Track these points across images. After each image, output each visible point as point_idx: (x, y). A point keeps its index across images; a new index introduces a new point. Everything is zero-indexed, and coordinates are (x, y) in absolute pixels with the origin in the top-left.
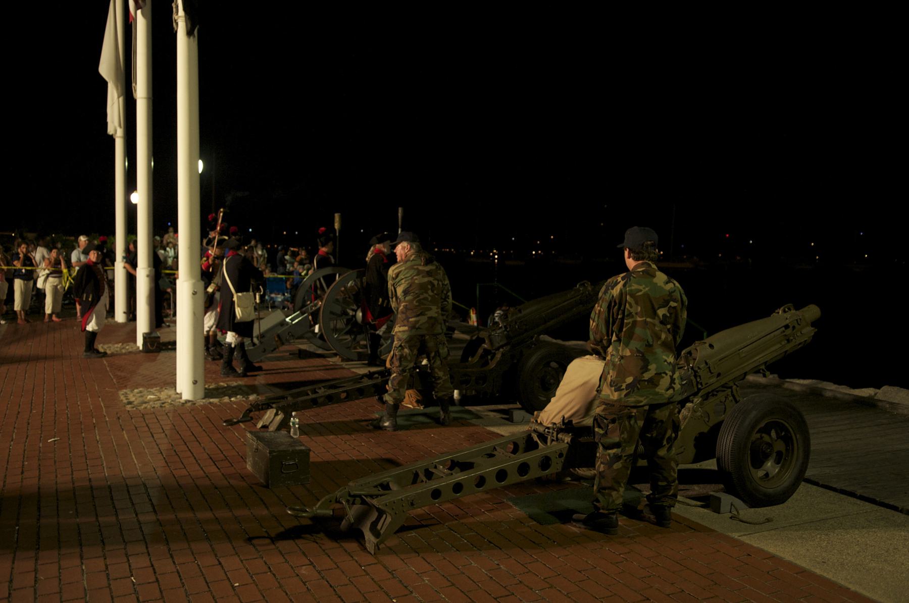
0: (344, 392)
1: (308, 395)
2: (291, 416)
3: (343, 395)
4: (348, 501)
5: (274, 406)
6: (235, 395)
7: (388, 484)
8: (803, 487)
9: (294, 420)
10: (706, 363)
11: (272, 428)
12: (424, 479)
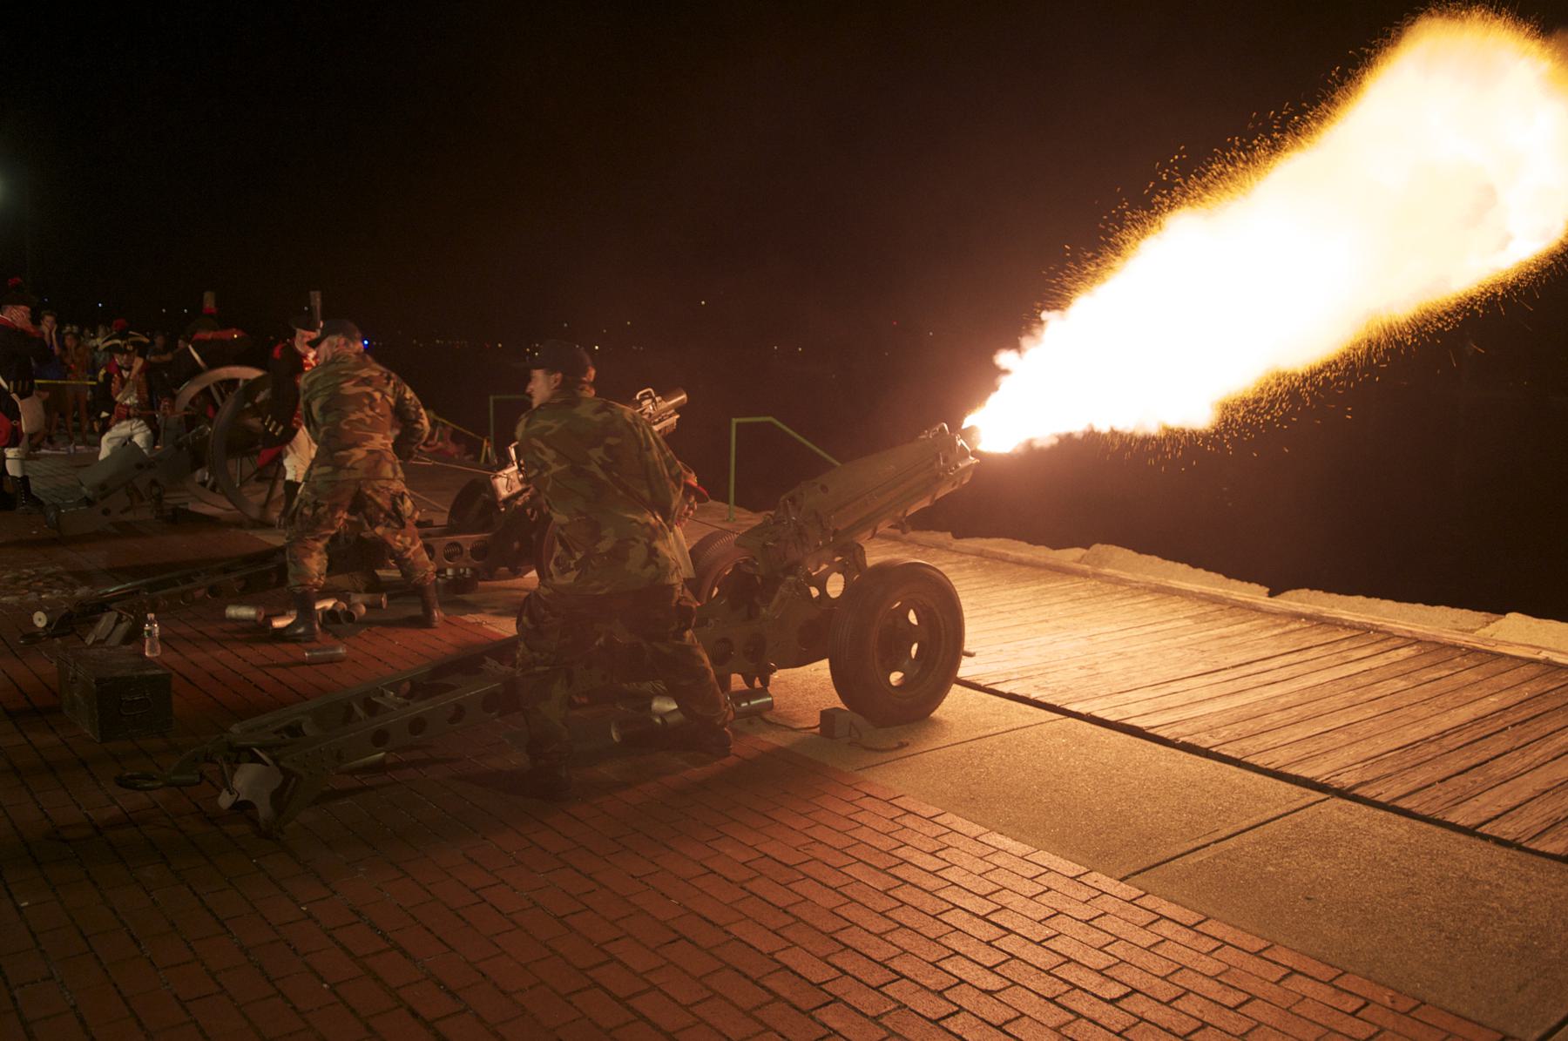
1: (176, 585)
2: (146, 620)
6: (50, 586)
11: (115, 639)
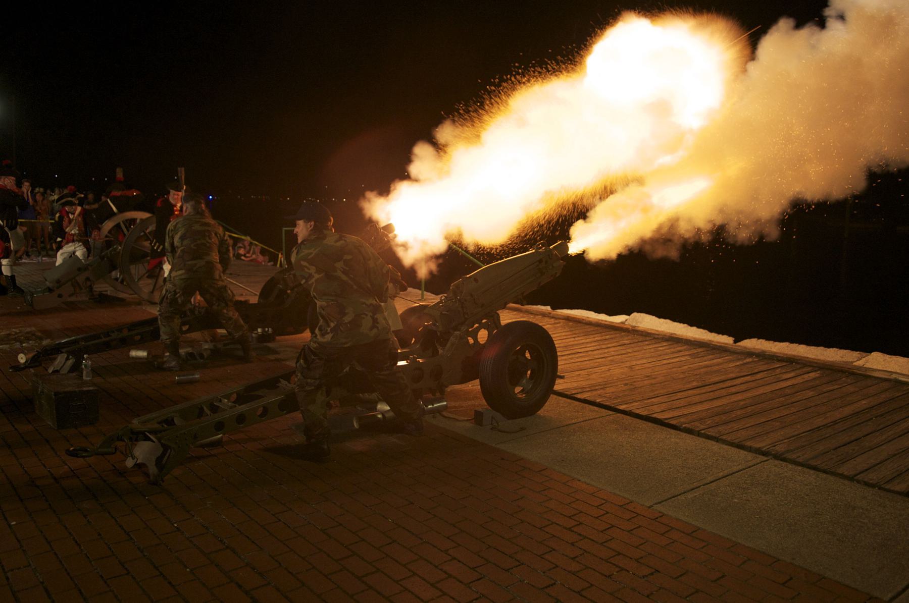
0: (137, 335)
2: (83, 359)
3: (138, 338)
4: (131, 439)
5: (64, 350)
7: (173, 420)
8: (553, 397)
9: (87, 362)
10: (472, 295)
11: (65, 371)
12: (209, 413)
